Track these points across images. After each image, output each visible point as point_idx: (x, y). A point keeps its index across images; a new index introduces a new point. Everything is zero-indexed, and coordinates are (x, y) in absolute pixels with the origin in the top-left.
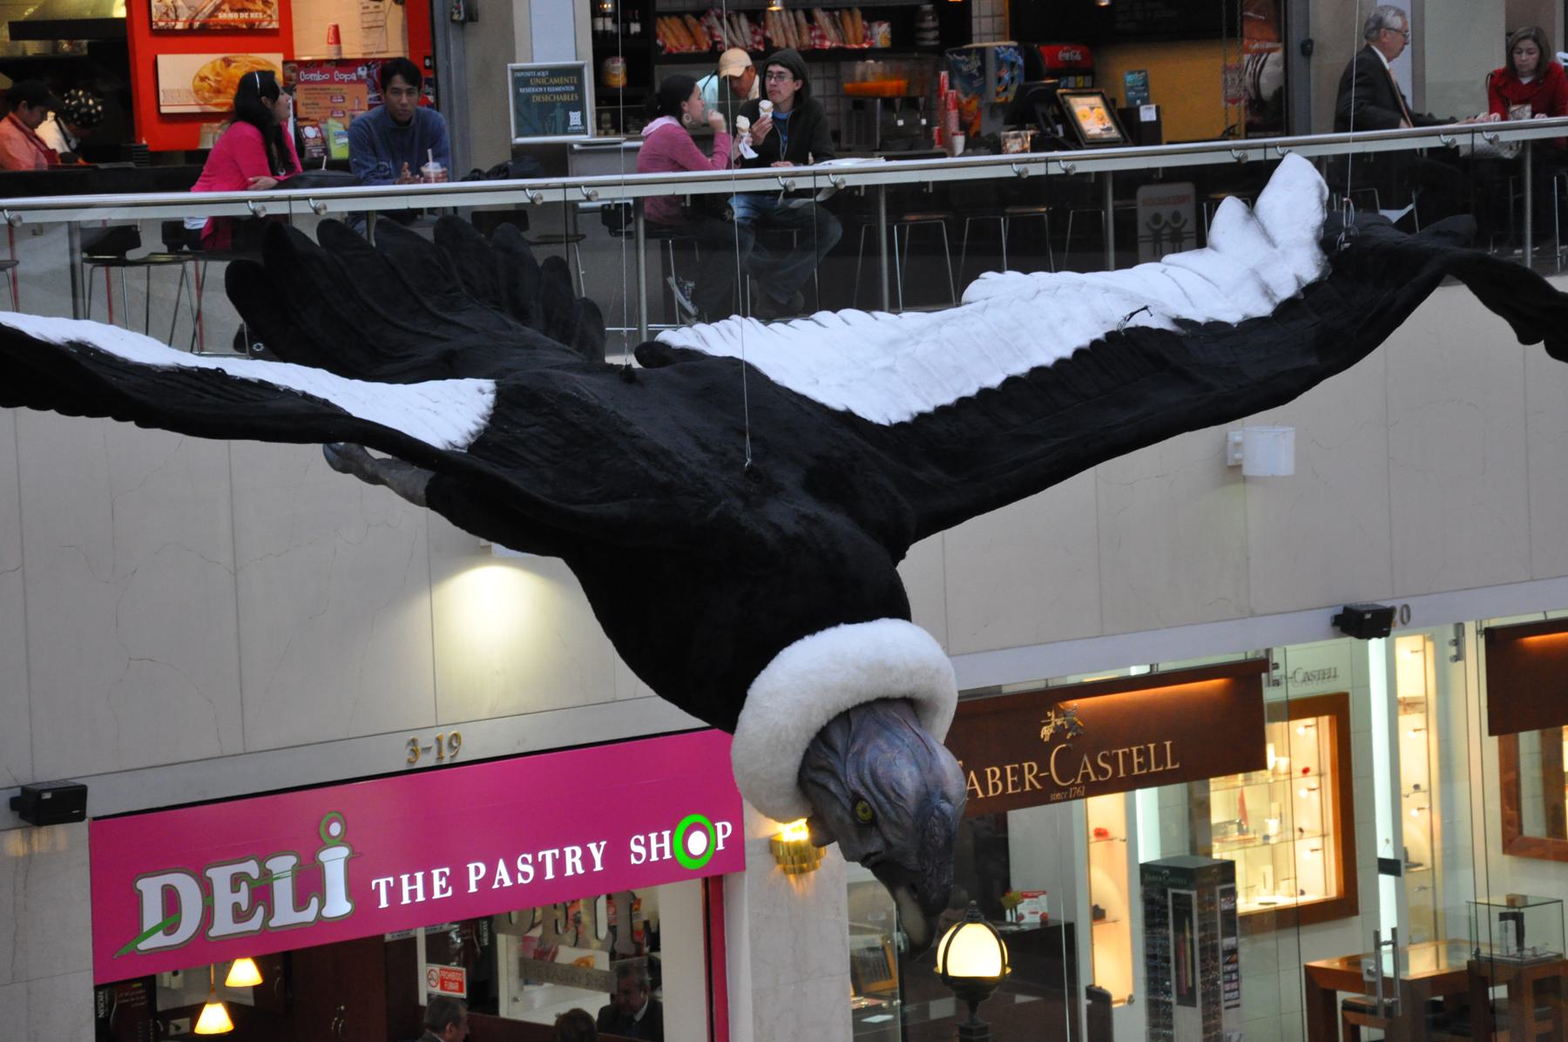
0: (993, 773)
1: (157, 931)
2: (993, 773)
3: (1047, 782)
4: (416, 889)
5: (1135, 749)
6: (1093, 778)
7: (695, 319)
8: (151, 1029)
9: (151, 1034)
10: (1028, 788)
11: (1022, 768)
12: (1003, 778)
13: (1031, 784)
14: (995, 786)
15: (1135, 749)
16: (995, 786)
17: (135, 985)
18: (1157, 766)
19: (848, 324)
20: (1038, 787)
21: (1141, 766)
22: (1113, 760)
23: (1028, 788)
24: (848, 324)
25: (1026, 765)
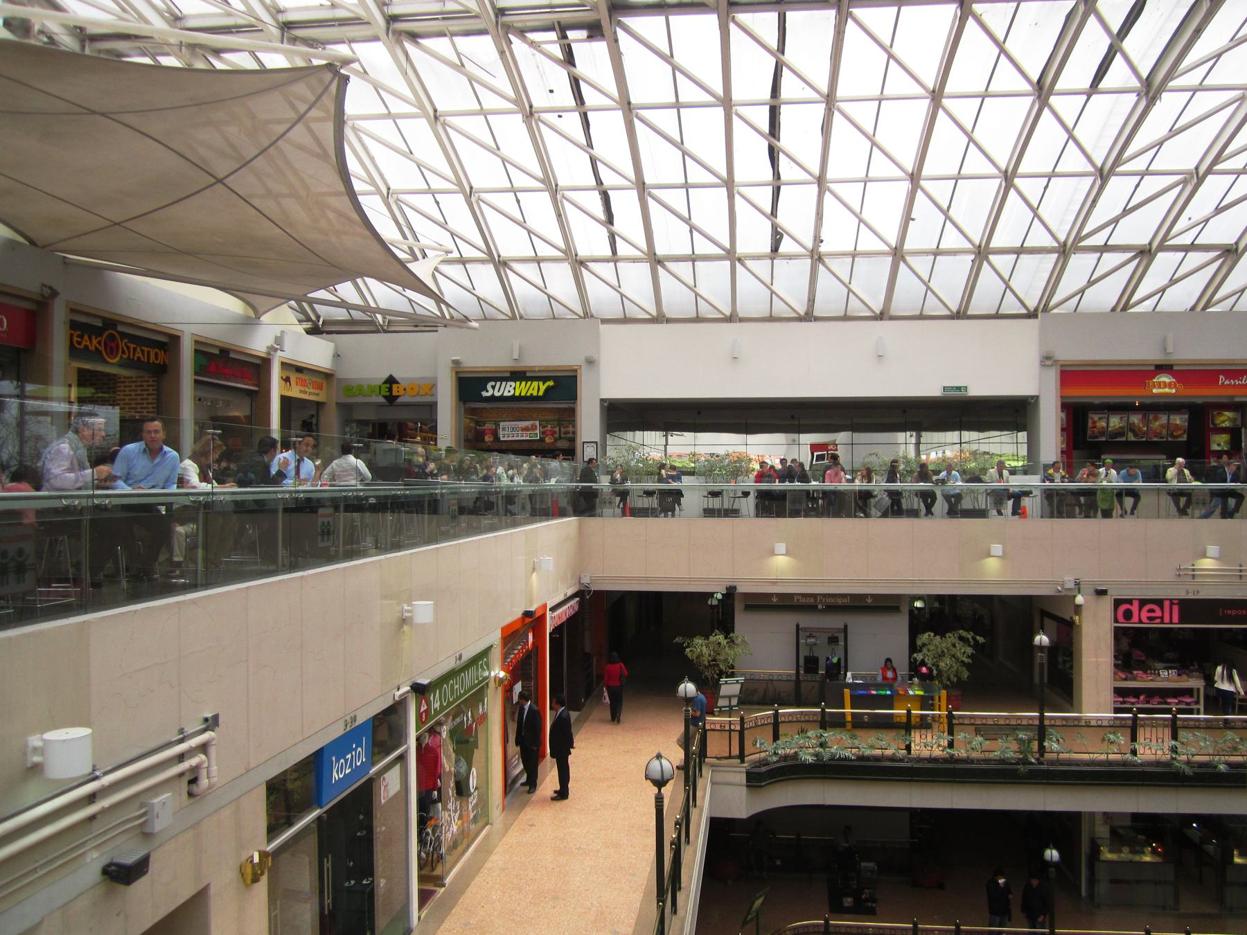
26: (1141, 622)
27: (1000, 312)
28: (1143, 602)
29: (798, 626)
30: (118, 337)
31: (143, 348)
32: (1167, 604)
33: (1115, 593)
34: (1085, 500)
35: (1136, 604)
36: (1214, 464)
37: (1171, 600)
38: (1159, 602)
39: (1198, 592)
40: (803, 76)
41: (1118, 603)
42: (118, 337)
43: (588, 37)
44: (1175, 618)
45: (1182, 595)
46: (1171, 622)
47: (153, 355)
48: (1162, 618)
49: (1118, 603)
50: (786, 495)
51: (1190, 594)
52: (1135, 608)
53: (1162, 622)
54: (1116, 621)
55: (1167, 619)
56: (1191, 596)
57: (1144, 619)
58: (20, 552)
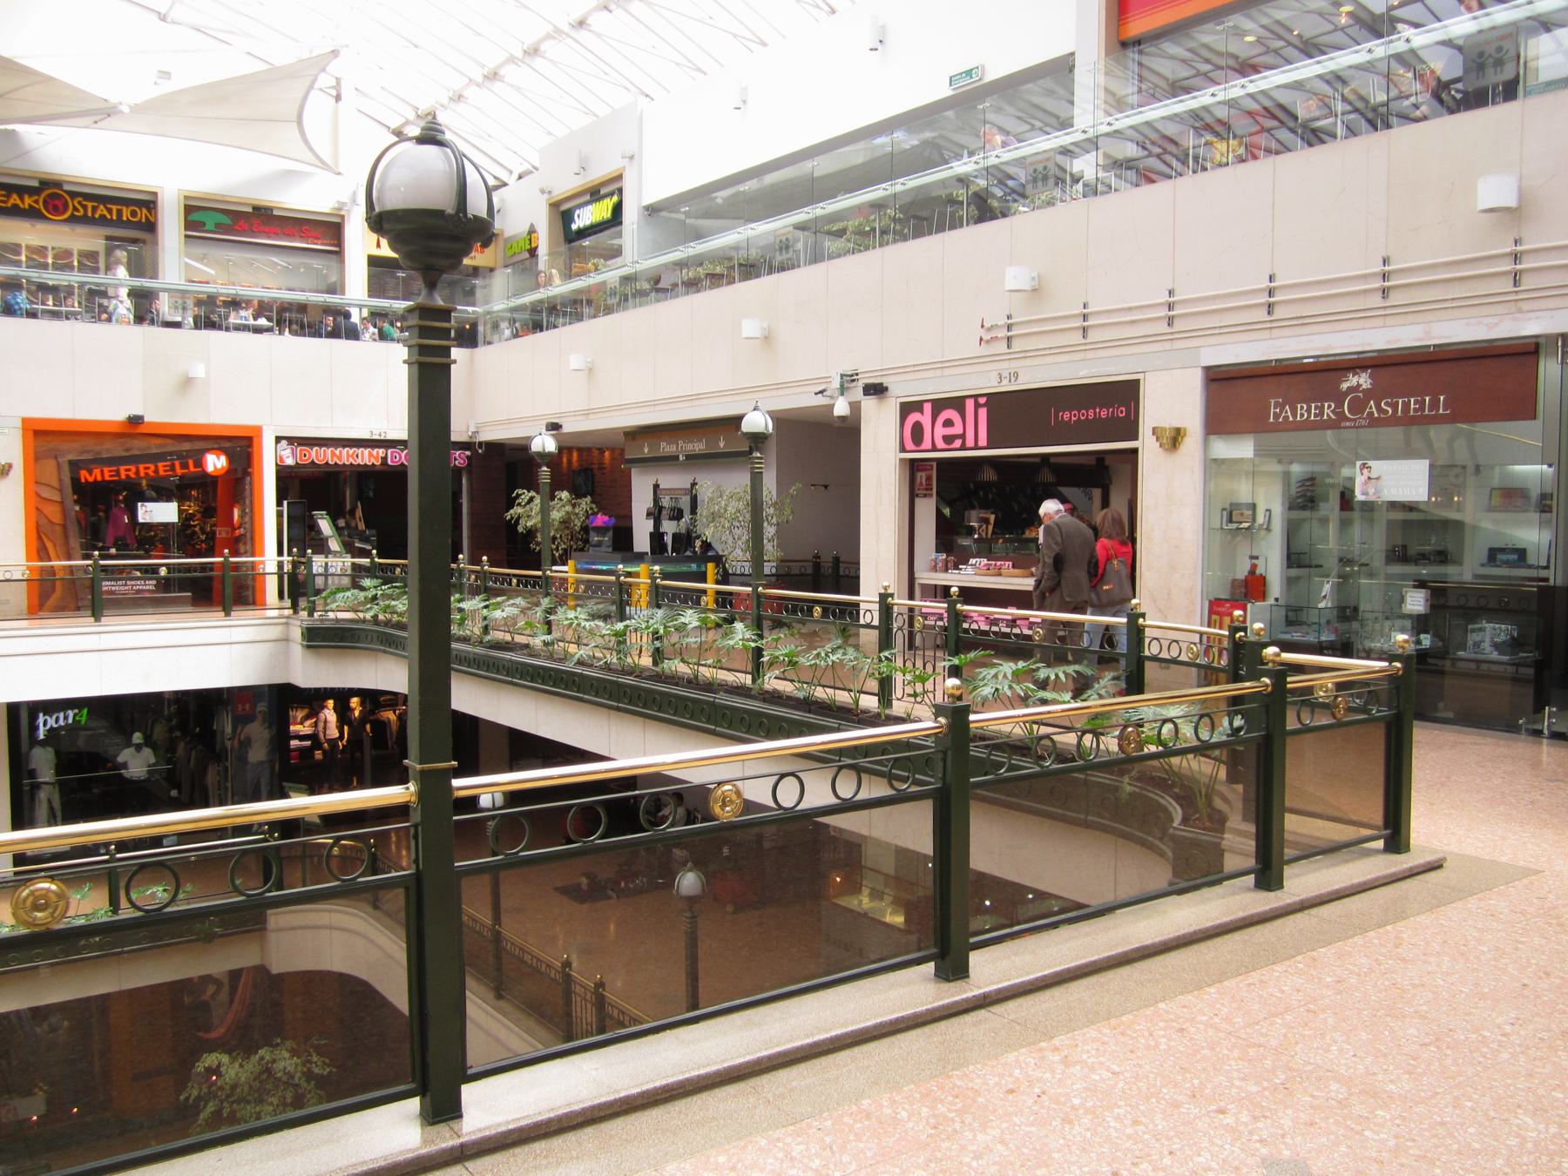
0: (1302, 408)
1: (445, 370)
2: (1302, 408)
3: (1341, 416)
4: (1135, 451)
5: (1412, 400)
6: (1376, 415)
7: (1399, 542)
8: (1104, 413)
9: (1104, 413)
10: (1325, 417)
11: (1323, 406)
12: (1309, 411)
13: (1328, 415)
14: (1302, 415)
15: (1412, 400)
16: (1302, 415)
17: (1352, 380)
18: (1430, 410)
19: (248, 53)
20: (1333, 417)
21: (1316, 415)
22: (1395, 406)
23: (1325, 417)
24: (248, 53)
25: (1326, 405)
26: (934, 449)
27: (877, 692)
28: (939, 405)
29: (656, 487)
30: (68, 198)
31: (109, 206)
32: (970, 404)
33: (902, 390)
34: (239, 878)
35: (928, 408)
36: (305, 729)
37: (976, 397)
38: (957, 403)
39: (1016, 375)
40: (568, 701)
41: (907, 409)
42: (68, 198)
43: (1072, 698)
44: (983, 441)
45: (988, 382)
46: (976, 448)
47: (143, 213)
48: (963, 436)
49: (907, 409)
50: (217, 481)
51: (1005, 382)
52: (925, 419)
53: (963, 448)
54: (903, 449)
55: (970, 442)
56: (1006, 387)
57: (940, 444)
58: (1045, 168)
